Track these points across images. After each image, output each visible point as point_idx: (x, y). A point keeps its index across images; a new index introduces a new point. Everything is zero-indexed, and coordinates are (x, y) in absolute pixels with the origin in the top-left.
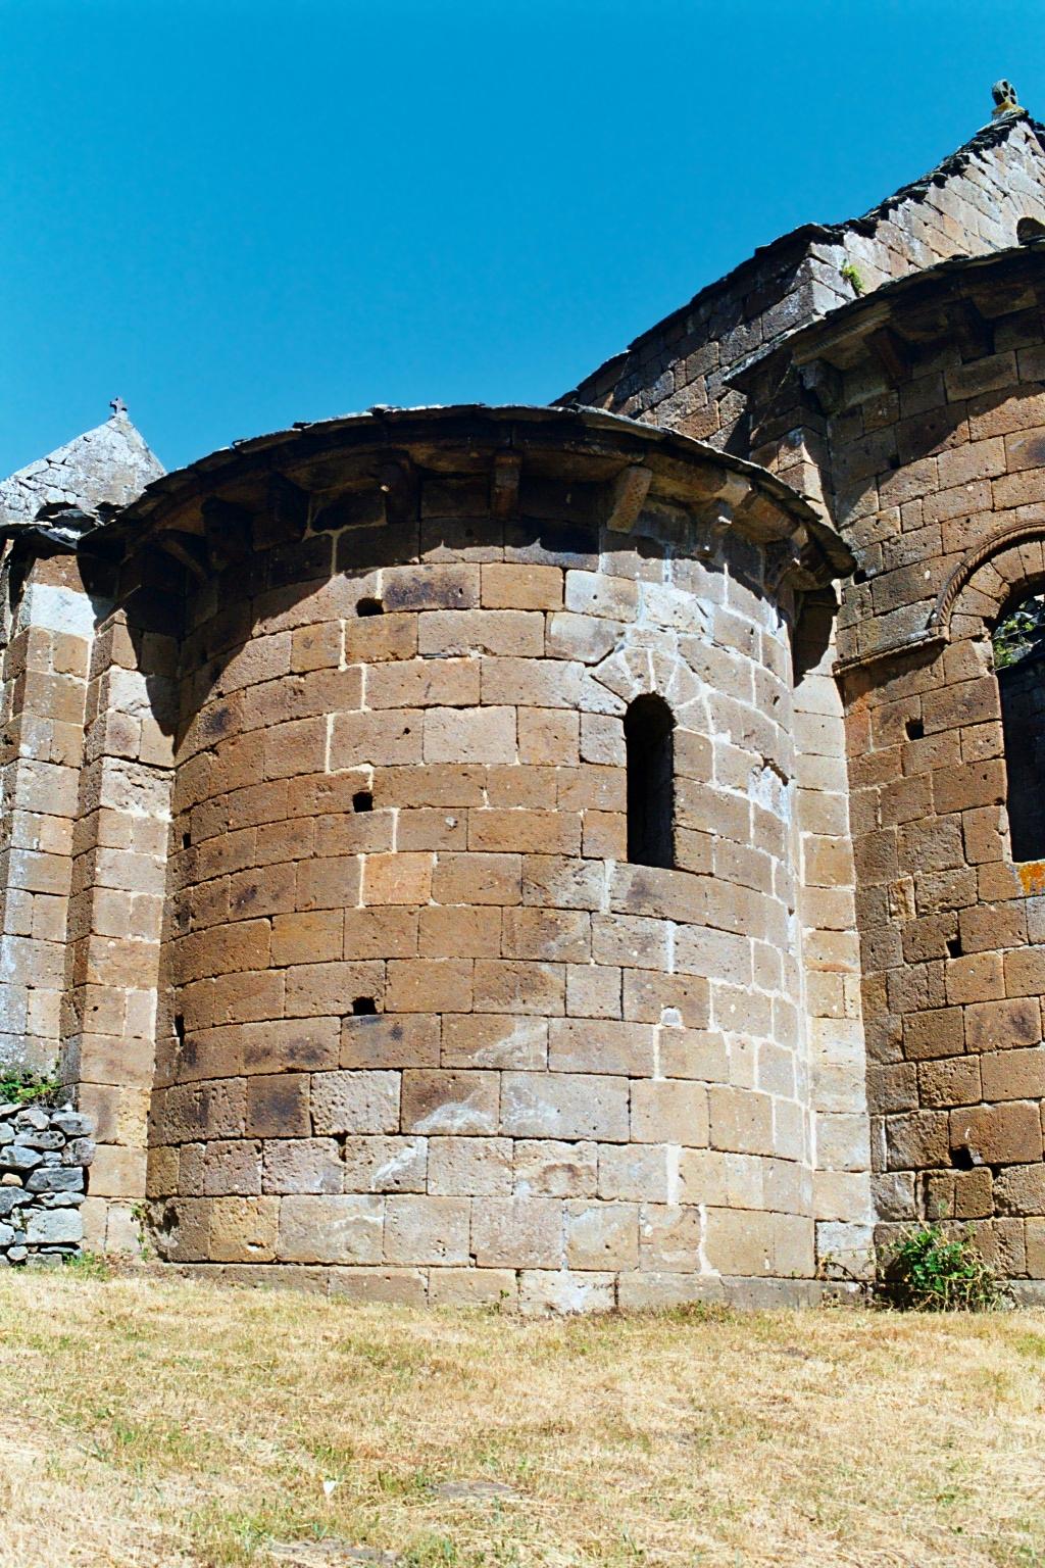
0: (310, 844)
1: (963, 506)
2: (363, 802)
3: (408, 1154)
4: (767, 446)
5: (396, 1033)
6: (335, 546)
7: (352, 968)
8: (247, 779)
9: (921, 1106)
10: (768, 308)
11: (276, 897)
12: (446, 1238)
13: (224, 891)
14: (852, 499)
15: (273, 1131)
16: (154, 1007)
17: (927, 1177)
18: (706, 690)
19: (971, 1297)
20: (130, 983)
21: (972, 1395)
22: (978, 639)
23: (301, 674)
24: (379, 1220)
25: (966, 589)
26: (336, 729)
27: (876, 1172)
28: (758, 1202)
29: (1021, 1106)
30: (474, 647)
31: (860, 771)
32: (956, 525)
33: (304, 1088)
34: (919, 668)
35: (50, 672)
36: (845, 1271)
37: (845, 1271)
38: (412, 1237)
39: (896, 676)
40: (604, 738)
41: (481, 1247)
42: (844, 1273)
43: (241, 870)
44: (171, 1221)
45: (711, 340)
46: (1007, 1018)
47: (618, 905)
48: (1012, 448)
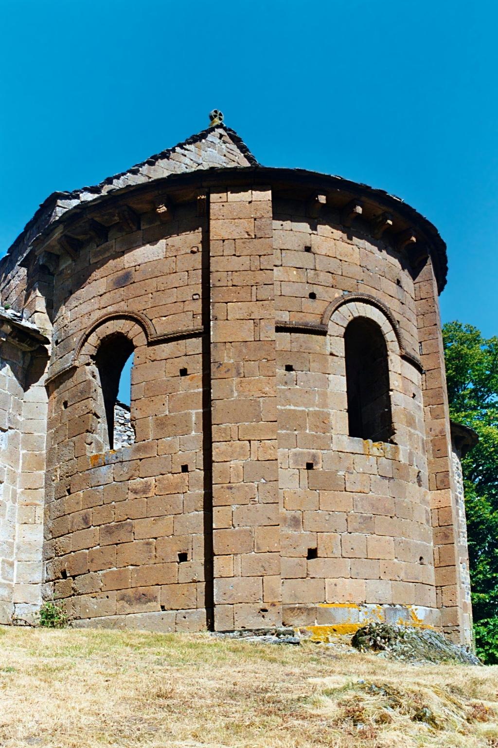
1: (89, 309)
17: (55, 583)
22: (88, 364)
25: (86, 344)
32: (86, 317)
36: (26, 622)
37: (26, 622)
42: (25, 623)
46: (81, 518)
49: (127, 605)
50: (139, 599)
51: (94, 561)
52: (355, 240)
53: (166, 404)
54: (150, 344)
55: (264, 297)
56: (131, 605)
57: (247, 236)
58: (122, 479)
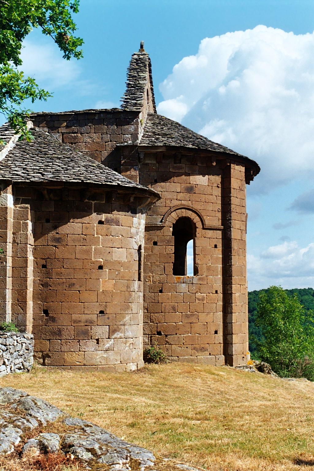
2: (101, 267)
3: (111, 343)
4: (127, 167)
6: (93, 206)
7: (100, 304)
9: (151, 322)
11: (81, 287)
12: (117, 359)
17: (151, 337)
19: (162, 361)
22: (171, 227)
23: (85, 235)
24: (106, 356)
25: (170, 216)
26: (95, 250)
29: (172, 324)
30: (120, 235)
32: (169, 201)
33: (89, 329)
34: (158, 230)
38: (112, 359)
39: (152, 230)
41: (122, 360)
43: (69, 279)
48: (182, 187)
49: (196, 352)
50: (201, 350)
51: (180, 330)
54: (204, 228)
58: (192, 292)
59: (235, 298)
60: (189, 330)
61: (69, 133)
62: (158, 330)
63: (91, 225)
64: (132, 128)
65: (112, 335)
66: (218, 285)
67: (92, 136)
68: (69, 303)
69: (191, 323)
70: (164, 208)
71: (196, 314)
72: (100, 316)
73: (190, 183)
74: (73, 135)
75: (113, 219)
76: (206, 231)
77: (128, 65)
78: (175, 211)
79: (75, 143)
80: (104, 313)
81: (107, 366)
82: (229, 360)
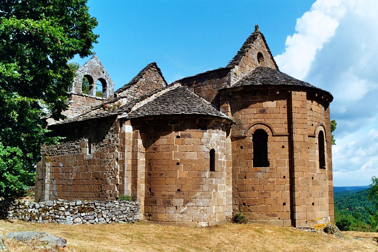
0: (171, 169)
1: (250, 117)
2: (178, 164)
3: (185, 209)
5: (183, 194)
8: (160, 158)
10: (223, 77)
11: (166, 175)
13: (157, 173)
14: (235, 112)
15: (167, 205)
16: (144, 186)
17: (240, 206)
18: (219, 147)
19: (245, 222)
20: (142, 184)
21: (252, 237)
22: (251, 136)
23: (169, 145)
24: (181, 217)
26: (174, 154)
27: (233, 205)
28: (222, 212)
30: (192, 143)
31: (233, 152)
33: (171, 200)
35: (128, 139)
38: (185, 219)
40: (207, 155)
41: (194, 219)
44: (150, 215)
45: (213, 79)
47: (209, 177)
52: (320, 105)
53: (279, 156)
54: (273, 136)
55: (306, 128)
56: (270, 217)
57: (301, 107)
59: (297, 181)
60: (264, 202)
61: (197, 87)
62: (244, 202)
63: (172, 139)
64: (227, 78)
65: (186, 204)
66: (286, 173)
67: (208, 87)
68: (160, 185)
69: (265, 198)
70: (246, 124)
71: (269, 192)
72: (177, 193)
73: (263, 107)
74: (199, 87)
75: (186, 134)
76: (275, 137)
77: (247, 39)
78: (253, 126)
79: (200, 92)
80: (180, 191)
81: (182, 223)
82: (294, 224)
